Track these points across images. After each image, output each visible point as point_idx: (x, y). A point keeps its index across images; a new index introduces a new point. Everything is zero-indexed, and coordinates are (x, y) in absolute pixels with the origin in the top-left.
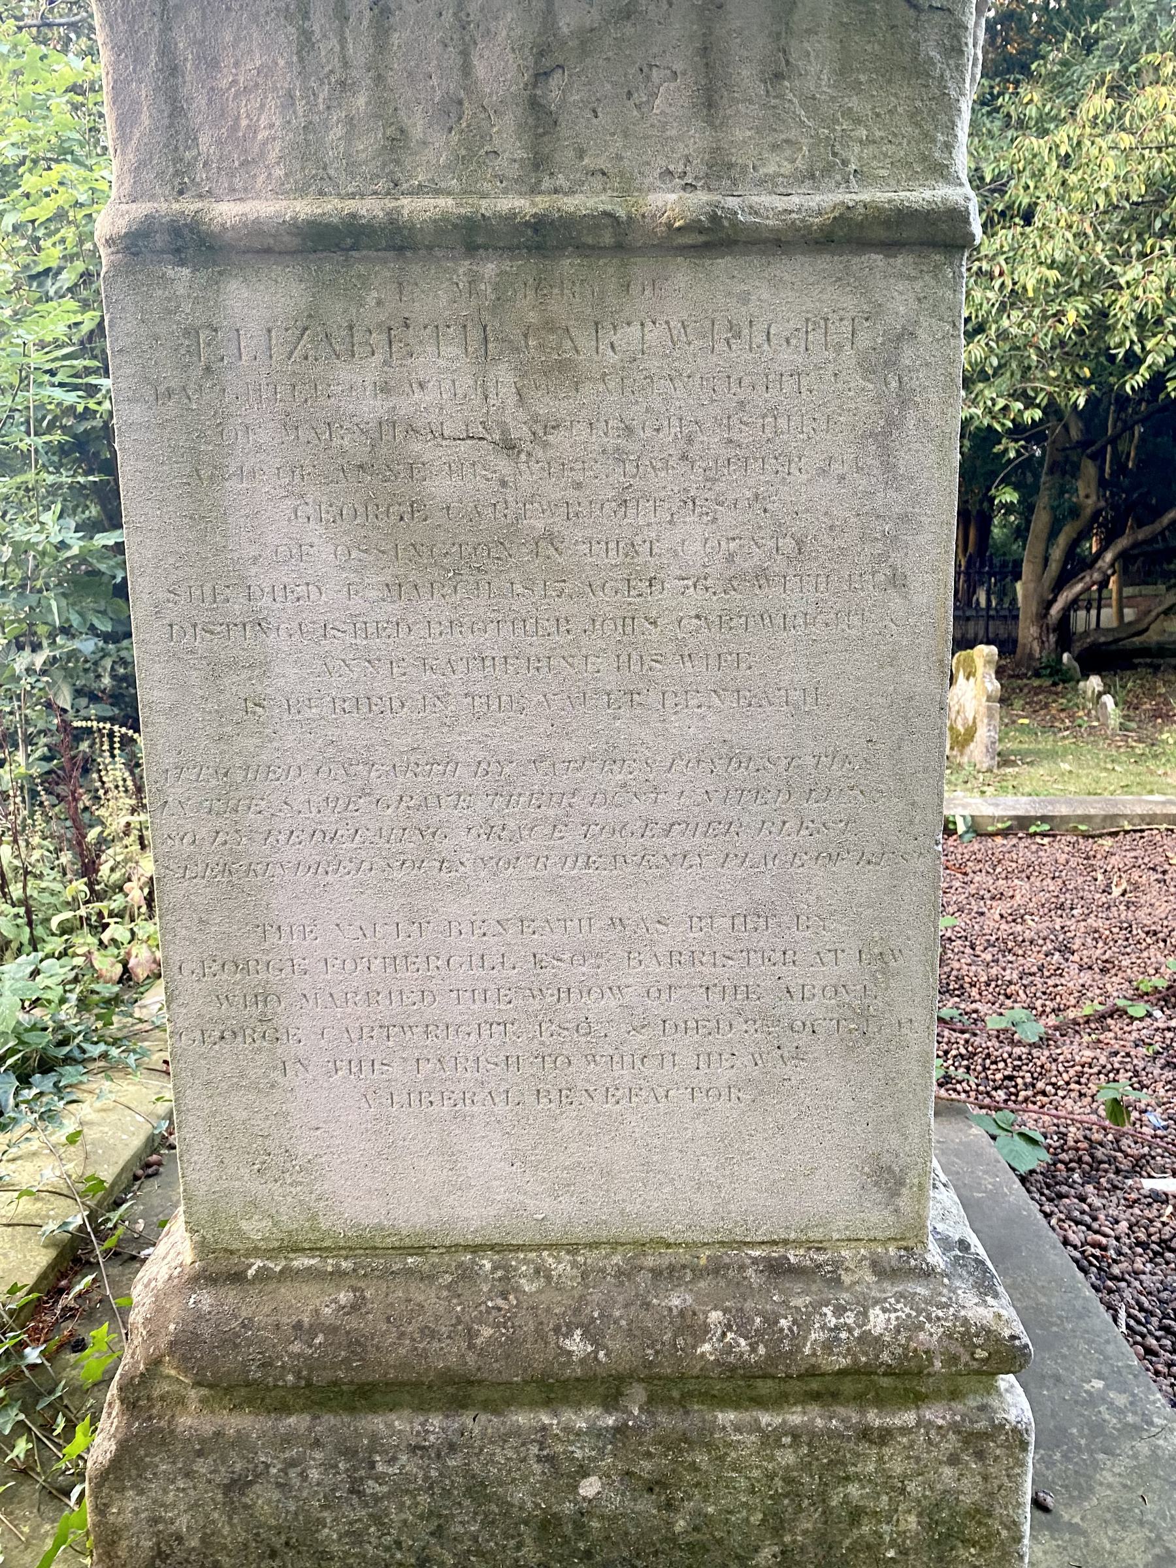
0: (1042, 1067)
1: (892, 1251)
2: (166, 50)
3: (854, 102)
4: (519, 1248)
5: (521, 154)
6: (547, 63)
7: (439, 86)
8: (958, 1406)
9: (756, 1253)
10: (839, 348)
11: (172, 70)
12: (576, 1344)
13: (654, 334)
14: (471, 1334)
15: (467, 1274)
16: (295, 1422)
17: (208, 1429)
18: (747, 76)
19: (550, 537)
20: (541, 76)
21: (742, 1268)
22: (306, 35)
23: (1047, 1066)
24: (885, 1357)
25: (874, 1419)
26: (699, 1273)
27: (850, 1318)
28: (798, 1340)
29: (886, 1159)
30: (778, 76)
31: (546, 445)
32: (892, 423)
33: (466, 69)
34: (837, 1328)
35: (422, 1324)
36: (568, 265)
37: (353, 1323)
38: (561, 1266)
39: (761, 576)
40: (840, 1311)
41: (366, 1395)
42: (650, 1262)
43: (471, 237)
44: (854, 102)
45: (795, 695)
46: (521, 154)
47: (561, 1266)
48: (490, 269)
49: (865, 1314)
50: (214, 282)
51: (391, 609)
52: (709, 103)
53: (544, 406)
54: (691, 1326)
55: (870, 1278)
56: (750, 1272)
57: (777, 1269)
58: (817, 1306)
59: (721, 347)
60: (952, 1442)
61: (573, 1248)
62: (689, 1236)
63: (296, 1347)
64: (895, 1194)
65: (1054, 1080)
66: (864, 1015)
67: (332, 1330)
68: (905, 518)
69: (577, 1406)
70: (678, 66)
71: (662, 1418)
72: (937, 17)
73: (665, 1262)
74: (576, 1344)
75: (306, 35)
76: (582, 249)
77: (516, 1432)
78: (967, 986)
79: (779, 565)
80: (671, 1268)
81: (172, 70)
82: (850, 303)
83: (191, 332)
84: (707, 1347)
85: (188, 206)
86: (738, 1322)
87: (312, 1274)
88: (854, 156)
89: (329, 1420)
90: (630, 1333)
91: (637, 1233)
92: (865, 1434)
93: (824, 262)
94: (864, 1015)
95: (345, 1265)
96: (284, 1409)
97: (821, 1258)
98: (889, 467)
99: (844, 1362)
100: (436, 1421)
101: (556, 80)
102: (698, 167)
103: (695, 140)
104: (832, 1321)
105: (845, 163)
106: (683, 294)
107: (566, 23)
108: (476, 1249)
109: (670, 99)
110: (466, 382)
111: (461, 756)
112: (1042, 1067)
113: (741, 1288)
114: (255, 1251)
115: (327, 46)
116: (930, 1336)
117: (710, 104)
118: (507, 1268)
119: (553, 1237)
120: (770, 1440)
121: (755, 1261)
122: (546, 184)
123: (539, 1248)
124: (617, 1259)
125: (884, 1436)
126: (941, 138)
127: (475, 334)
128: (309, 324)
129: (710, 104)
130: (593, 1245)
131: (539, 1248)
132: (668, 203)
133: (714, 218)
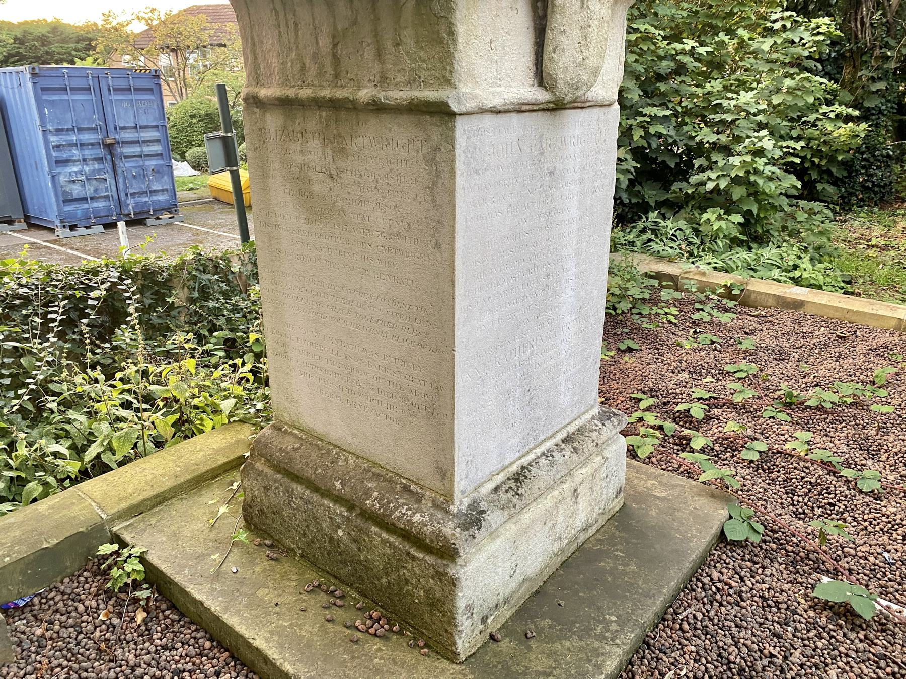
0: (856, 506)
1: (442, 499)
2: (252, 38)
3: (422, 54)
4: (345, 450)
5: (332, 73)
6: (336, 41)
7: (311, 49)
8: (439, 561)
9: (403, 481)
10: (418, 152)
11: (254, 44)
12: (338, 485)
13: (367, 140)
14: (316, 470)
15: (329, 452)
16: (278, 476)
17: (261, 469)
18: (389, 45)
19: (342, 210)
20: (335, 45)
21: (397, 484)
22: (280, 32)
23: (859, 507)
24: (413, 530)
25: (412, 551)
26: (385, 480)
27: (409, 513)
28: (392, 512)
29: (440, 464)
30: (398, 45)
31: (340, 177)
32: (435, 183)
33: (317, 43)
34: (404, 514)
35: (309, 463)
36: (343, 114)
37: (293, 453)
38: (352, 460)
39: (398, 235)
40: (409, 509)
41: (296, 478)
42: (374, 470)
43: (318, 103)
44: (422, 54)
45: (410, 282)
46: (332, 73)
47: (352, 460)
48: (324, 114)
49: (414, 514)
50: (264, 113)
51: (306, 227)
52: (379, 54)
53: (341, 164)
54: (368, 493)
55: (430, 505)
56: (398, 486)
57: (406, 489)
58: (403, 504)
59: (384, 147)
60: (432, 571)
61: (357, 457)
62: (387, 467)
63: (278, 454)
64: (443, 479)
65: (857, 515)
66: (432, 407)
67: (287, 453)
68: (439, 222)
69: (342, 506)
70: (370, 41)
71: (359, 520)
72: (443, 20)
73: (378, 472)
74: (338, 485)
75: (280, 32)
76: (348, 109)
77: (323, 505)
78: (883, 450)
79: (403, 233)
80: (378, 475)
81: (254, 44)
82: (421, 135)
83: (260, 130)
84: (368, 502)
85: (256, 90)
86: (379, 499)
87: (296, 436)
88: (423, 74)
89: (286, 480)
90: (352, 488)
91: (376, 460)
92: (408, 554)
93: (413, 118)
94: (432, 407)
95: (304, 437)
96: (279, 472)
97: (419, 491)
98: (434, 201)
99: (402, 526)
100: (307, 492)
101: (339, 47)
102: (378, 79)
103: (376, 69)
104: (404, 511)
105: (420, 78)
106: (373, 125)
107: (340, 27)
108: (335, 446)
109: (369, 54)
110: (320, 153)
111: (324, 280)
112: (856, 506)
113: (392, 490)
114: (286, 424)
115: (285, 36)
116: (428, 530)
117: (379, 55)
118: (339, 455)
119: (352, 451)
120: (384, 542)
121: (401, 483)
122: (339, 84)
123: (350, 453)
124: (366, 465)
125: (413, 558)
126: (449, 68)
127: (322, 137)
128: (284, 128)
129: (379, 55)
130: (363, 458)
131: (350, 453)
132: (365, 94)
133: (374, 101)
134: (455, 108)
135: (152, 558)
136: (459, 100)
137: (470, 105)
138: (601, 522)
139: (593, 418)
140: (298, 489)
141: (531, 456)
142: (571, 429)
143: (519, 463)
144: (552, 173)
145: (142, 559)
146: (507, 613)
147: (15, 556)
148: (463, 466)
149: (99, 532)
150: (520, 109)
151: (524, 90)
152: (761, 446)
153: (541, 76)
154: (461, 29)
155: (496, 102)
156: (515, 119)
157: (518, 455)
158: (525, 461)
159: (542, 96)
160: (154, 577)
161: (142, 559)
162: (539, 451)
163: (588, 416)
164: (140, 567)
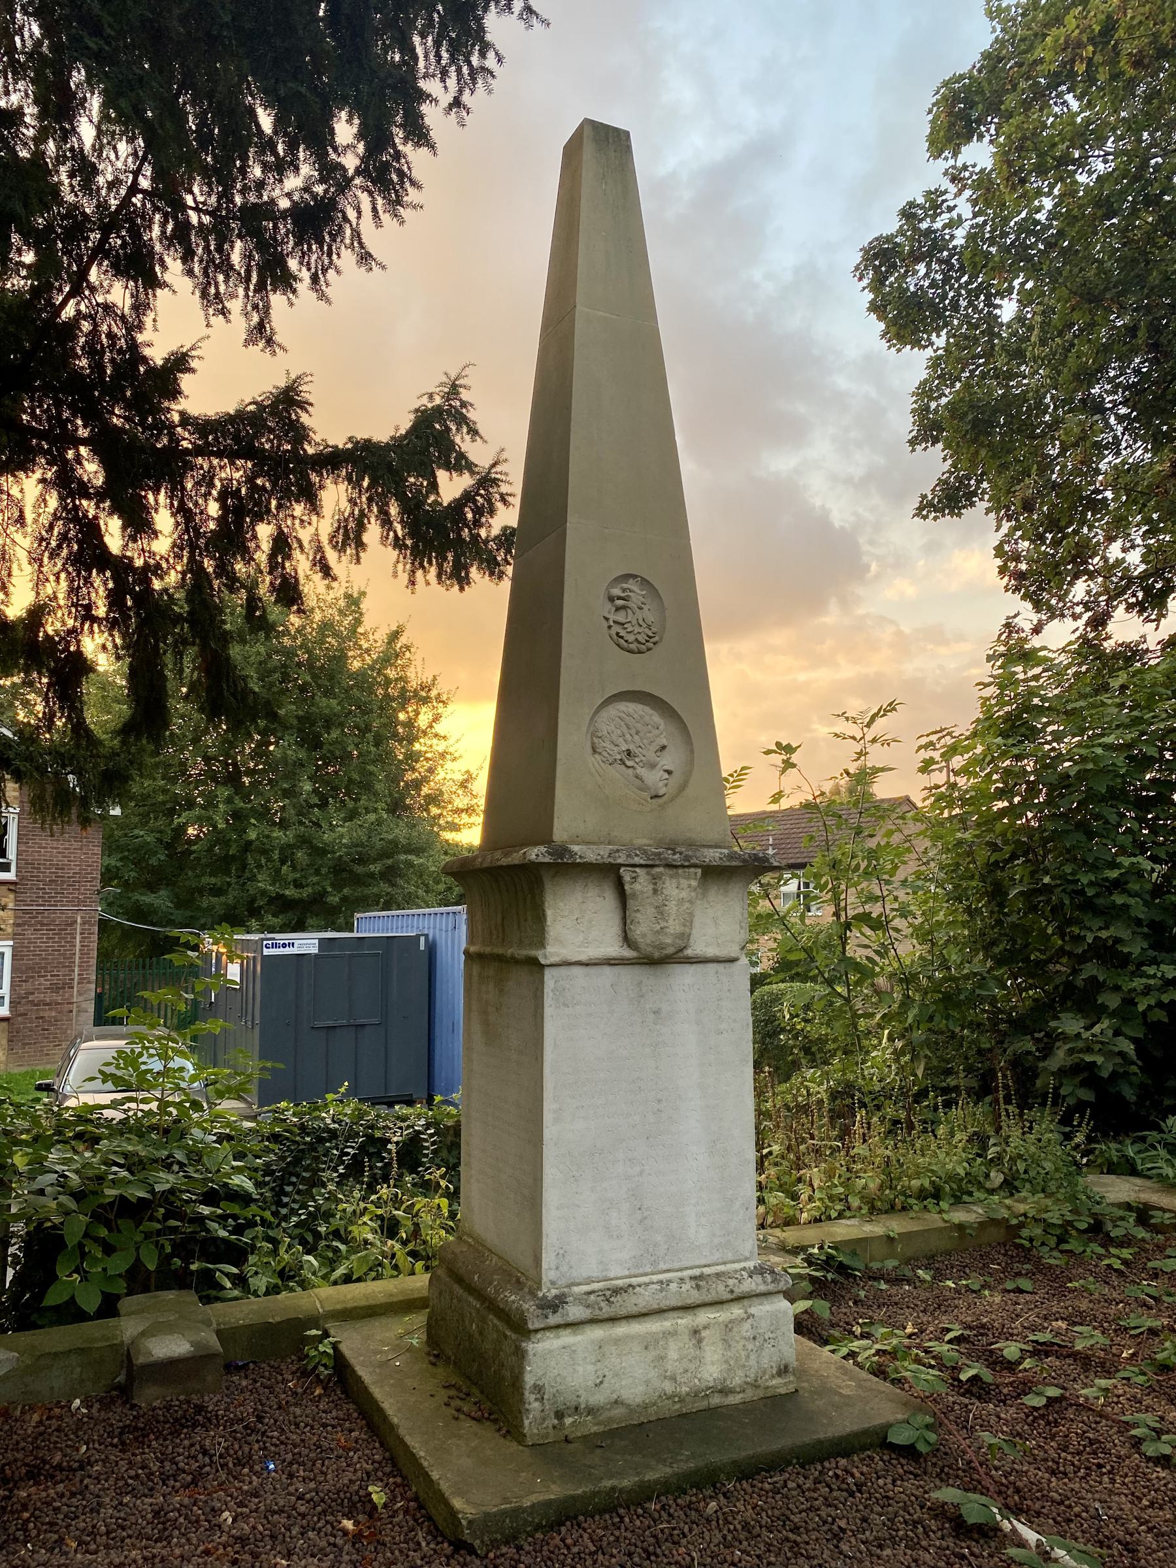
120: (495, 1326)
134: (543, 961)
135: (343, 1347)
136: (545, 957)
137: (553, 960)
138: (750, 1395)
139: (744, 1269)
140: (493, 1320)
141: (646, 1279)
142: (707, 1271)
143: (627, 1281)
144: (656, 1012)
145: (335, 1346)
146: (592, 1427)
147: (248, 1322)
148: (552, 1256)
149: (313, 1321)
150: (610, 962)
151: (614, 948)
152: (1053, 1392)
153: (627, 939)
154: (549, 913)
155: (583, 958)
156: (607, 970)
157: (627, 1273)
158: (634, 1281)
159: (628, 953)
160: (340, 1364)
161: (335, 1346)
162: (655, 1278)
163: (737, 1266)
164: (331, 1351)
